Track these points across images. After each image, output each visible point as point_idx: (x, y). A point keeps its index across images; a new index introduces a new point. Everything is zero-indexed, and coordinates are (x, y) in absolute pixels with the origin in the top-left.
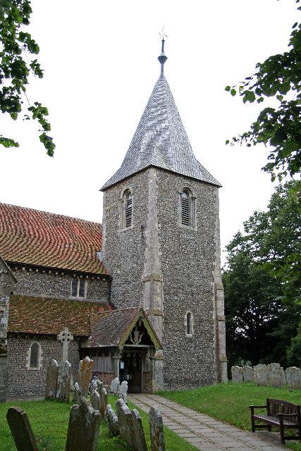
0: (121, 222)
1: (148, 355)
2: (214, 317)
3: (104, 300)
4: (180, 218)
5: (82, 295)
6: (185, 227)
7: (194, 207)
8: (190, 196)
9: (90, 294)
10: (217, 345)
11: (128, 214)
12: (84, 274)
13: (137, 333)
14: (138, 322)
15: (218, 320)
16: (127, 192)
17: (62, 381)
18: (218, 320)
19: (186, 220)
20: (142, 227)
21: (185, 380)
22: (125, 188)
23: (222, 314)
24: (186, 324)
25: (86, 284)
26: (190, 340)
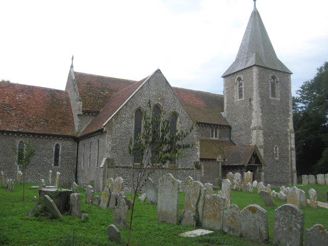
0: (236, 95)
1: (258, 169)
2: (289, 148)
3: (227, 139)
4: (270, 93)
5: (216, 137)
6: (272, 98)
7: (278, 87)
8: (275, 80)
9: (220, 137)
10: (291, 163)
11: (240, 91)
12: (217, 125)
13: (253, 158)
14: (254, 153)
15: (292, 149)
16: (239, 79)
17: (236, 181)
18: (292, 149)
19: (274, 95)
20: (250, 99)
21: (275, 182)
22: (238, 76)
23: (293, 146)
24: (275, 152)
25: (218, 130)
26: (277, 161)
